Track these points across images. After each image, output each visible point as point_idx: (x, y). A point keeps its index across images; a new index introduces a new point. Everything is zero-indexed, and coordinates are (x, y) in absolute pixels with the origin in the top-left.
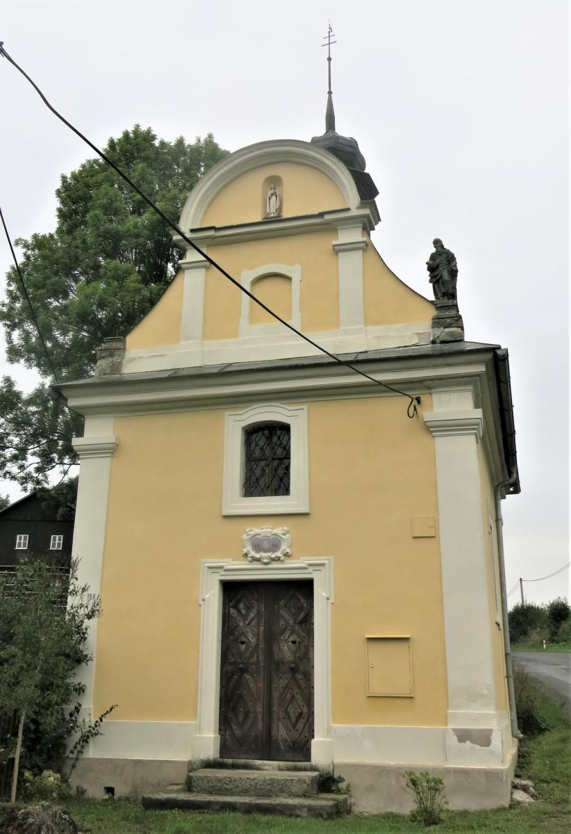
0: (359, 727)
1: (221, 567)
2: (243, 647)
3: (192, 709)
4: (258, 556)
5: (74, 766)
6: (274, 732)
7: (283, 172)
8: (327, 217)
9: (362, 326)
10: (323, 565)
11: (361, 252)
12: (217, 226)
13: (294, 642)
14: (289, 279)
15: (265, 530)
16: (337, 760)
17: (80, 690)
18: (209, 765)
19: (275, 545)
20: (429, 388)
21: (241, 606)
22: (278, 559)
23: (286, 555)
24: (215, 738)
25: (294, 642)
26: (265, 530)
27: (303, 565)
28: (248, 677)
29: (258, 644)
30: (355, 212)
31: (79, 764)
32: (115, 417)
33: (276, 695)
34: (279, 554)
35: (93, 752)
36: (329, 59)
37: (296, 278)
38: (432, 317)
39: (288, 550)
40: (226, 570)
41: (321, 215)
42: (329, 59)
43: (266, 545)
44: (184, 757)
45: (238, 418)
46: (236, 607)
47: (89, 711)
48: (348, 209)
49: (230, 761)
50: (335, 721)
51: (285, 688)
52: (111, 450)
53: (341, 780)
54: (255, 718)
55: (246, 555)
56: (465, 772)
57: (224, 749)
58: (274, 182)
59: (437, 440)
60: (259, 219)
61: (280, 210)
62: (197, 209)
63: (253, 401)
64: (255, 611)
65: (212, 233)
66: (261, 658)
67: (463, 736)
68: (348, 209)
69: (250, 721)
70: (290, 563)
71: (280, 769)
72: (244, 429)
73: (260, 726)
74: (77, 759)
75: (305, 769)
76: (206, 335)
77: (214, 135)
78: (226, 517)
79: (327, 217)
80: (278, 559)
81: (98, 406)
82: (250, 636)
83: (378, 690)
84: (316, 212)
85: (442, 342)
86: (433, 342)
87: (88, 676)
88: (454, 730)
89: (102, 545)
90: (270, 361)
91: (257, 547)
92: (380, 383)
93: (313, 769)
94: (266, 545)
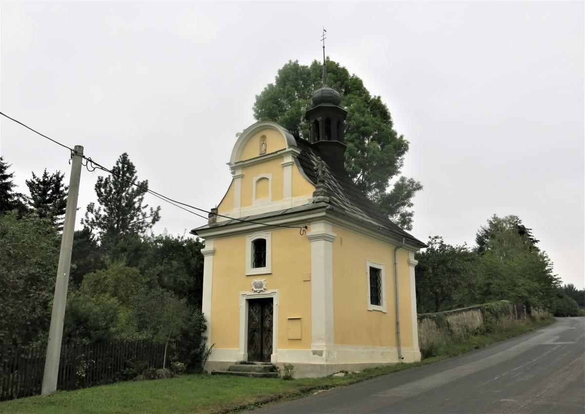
0: (285, 350)
1: (245, 295)
2: (255, 323)
3: (238, 345)
4: (256, 290)
5: (204, 364)
6: (263, 352)
7: (264, 133)
8: (278, 153)
9: (291, 198)
10: (276, 292)
11: (291, 166)
12: (244, 160)
13: (269, 321)
14: (268, 179)
15: (257, 280)
16: (278, 361)
17: (206, 339)
18: (242, 363)
19: (261, 286)
20: (310, 222)
21: (254, 308)
22: (262, 291)
23: (264, 289)
24: (244, 354)
25: (269, 321)
26: (257, 280)
27: (269, 293)
28: (256, 333)
29: (259, 321)
30: (288, 150)
31: (206, 363)
32: (324, 222)
33: (264, 339)
34: (262, 289)
35: (210, 359)
36: (324, 47)
37: (270, 179)
38: (313, 192)
39: (265, 288)
40: (248, 295)
41: (276, 152)
42: (324, 47)
43: (258, 286)
44: (235, 361)
45: (250, 238)
46: (252, 308)
47: (209, 345)
48: (285, 149)
49: (251, 362)
50: (279, 348)
51: (267, 337)
52: (213, 253)
53: (278, 368)
54: (258, 349)
55: (253, 289)
56: (314, 365)
57: (249, 358)
58: (264, 137)
59: (312, 243)
60: (258, 156)
61: (265, 150)
62: (237, 154)
63: (254, 231)
64: (258, 309)
65: (241, 163)
66: (260, 327)
67: (315, 353)
68: (285, 149)
69: (256, 349)
70: (266, 292)
71: (262, 365)
72: (252, 242)
73: (259, 350)
74: (205, 361)
75: (269, 364)
76: (241, 206)
77: (330, 57)
78: (247, 276)
79: (278, 153)
80: (262, 291)
81: (316, 218)
82: (257, 319)
83: (290, 337)
84: (274, 151)
85: (317, 202)
86: (313, 203)
87: (209, 334)
88: (312, 351)
89: (211, 288)
90: (275, 212)
91: (256, 287)
92: (271, 225)
93: (271, 364)
94: (258, 286)
